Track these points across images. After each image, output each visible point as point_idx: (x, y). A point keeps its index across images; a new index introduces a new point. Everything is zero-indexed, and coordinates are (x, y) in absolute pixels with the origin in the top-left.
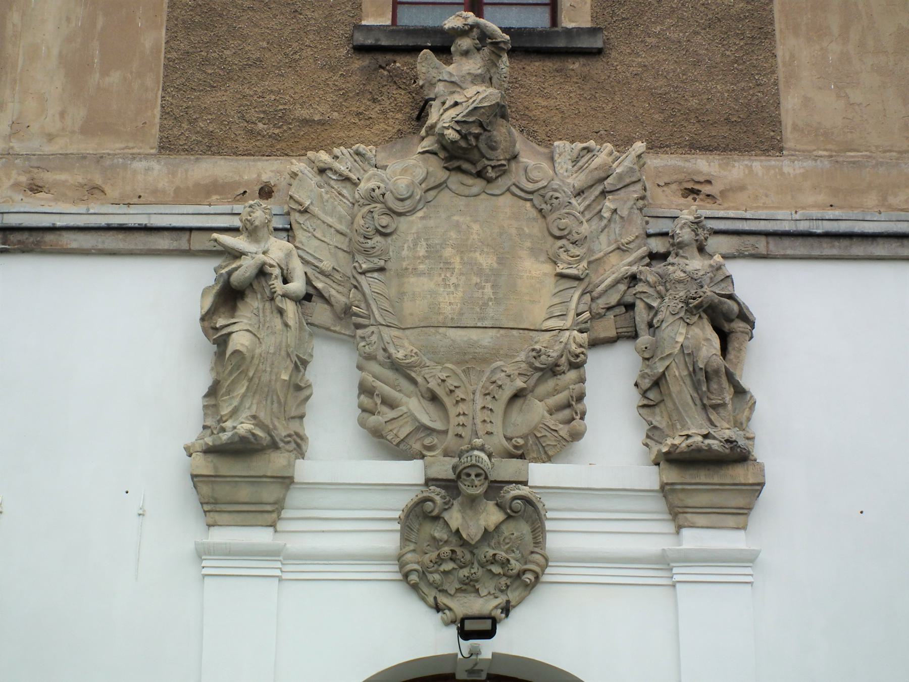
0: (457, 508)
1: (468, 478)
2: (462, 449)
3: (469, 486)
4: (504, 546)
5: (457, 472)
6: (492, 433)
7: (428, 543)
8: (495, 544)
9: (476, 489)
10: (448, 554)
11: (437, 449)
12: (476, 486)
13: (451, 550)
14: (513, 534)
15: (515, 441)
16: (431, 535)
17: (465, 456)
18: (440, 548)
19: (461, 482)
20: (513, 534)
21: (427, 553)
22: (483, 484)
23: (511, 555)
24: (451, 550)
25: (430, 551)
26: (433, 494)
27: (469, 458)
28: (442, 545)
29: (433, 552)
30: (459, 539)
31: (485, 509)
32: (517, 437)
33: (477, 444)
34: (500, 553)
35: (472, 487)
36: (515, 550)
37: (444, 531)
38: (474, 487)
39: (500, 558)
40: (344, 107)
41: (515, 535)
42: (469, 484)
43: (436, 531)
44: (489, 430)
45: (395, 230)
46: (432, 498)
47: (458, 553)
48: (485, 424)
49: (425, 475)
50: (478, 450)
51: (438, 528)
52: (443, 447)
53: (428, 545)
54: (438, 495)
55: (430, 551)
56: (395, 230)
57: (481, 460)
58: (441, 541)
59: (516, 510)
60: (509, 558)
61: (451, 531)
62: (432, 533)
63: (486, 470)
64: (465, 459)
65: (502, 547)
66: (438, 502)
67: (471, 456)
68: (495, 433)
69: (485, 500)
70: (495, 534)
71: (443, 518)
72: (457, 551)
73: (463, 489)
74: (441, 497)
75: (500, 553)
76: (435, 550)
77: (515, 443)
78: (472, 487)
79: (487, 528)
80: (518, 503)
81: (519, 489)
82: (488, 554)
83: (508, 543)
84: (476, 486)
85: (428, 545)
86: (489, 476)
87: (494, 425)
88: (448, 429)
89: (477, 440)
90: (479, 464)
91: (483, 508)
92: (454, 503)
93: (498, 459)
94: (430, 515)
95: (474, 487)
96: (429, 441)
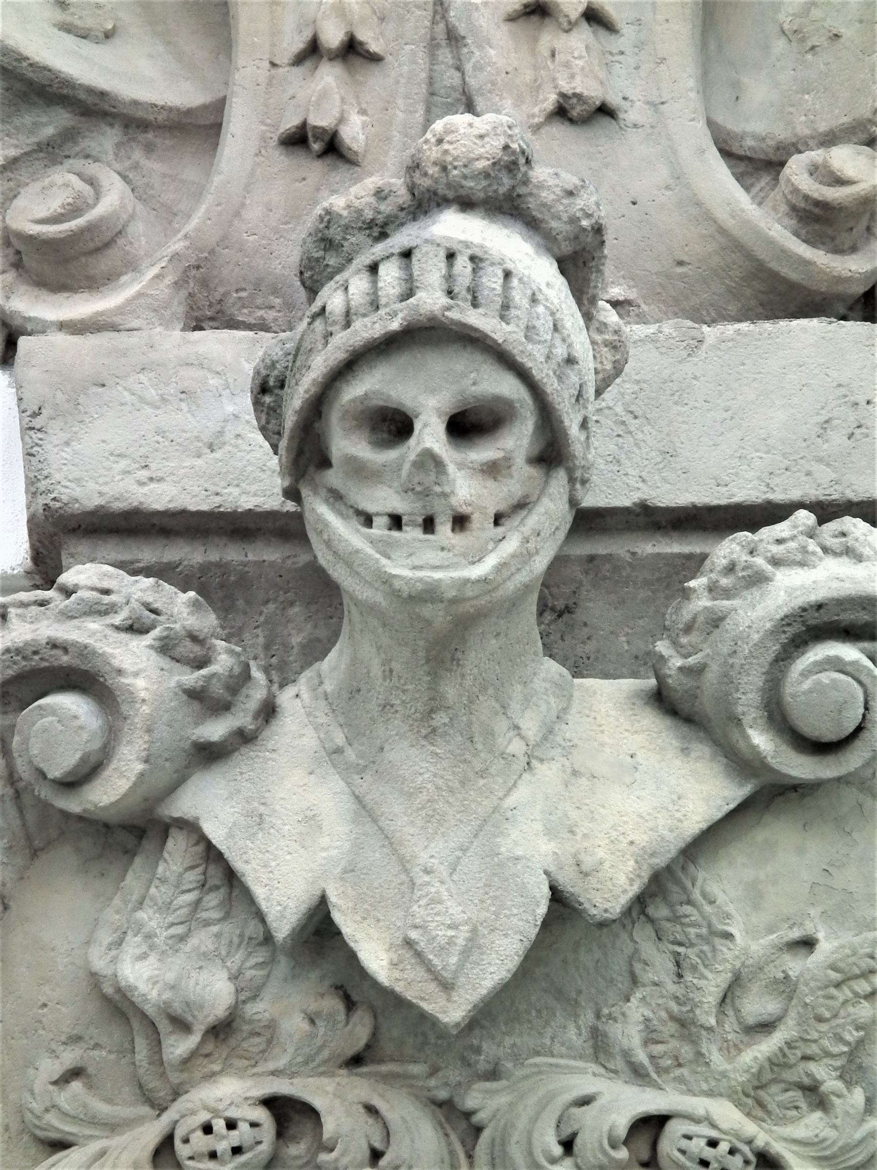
0: (310, 740)
1: (391, 455)
2: (329, 218)
3: (396, 522)
4: (731, 1050)
5: (290, 419)
6: (605, 111)
7: (70, 1057)
8: (650, 1038)
9: (458, 540)
10: (242, 1134)
11: (132, 265)
12: (460, 522)
13: (271, 1103)
14: (808, 944)
15: (814, 170)
16: (94, 979)
17: (364, 259)
18: (177, 1094)
19: (336, 497)
20: (808, 944)
21: (59, 1145)
22: (522, 505)
23: (800, 1131)
24: (271, 1103)
25: (94, 1121)
26: (94, 625)
27: (390, 273)
28: (186, 1062)
29: (113, 1127)
30: (334, 1004)
31: (548, 732)
32: (829, 140)
33: (455, 150)
34: (699, 1105)
35: (429, 525)
36: (831, 1084)
37: (203, 939)
38: (444, 529)
39: (698, 1146)
40: (591, 891)
41: (825, 947)
42: (398, 504)
43: (133, 945)
44: (579, 86)
45: (379, 654)
46: (84, 651)
47: (329, 1126)
48: (548, 38)
49: (31, 483)
50: (466, 204)
51: (149, 917)
52: (177, 245)
53: (76, 1073)
54: (135, 628)
55: (94, 1121)
56: (379, 654)
57: (492, 281)
58: (182, 1025)
59: (828, 733)
60: (779, 1148)
61: (268, 939)
62: (99, 963)
63: (543, 373)
64: (359, 285)
65: (716, 1058)
66: (141, 685)
67: (407, 254)
68: (632, 114)
69: (552, 668)
70: (643, 935)
71: (191, 827)
72: (317, 1103)
73: (349, 559)
74: (165, 648)
75: (699, 1105)
76: (146, 1110)
77: (808, 185)
78: (429, 525)
79: (568, 881)
80: (837, 665)
81: (849, 552)
82: (587, 1114)
83: (766, 1027)
84: (460, 522)
85: (76, 1073)
86: (574, 430)
87: (628, 35)
88: (219, 106)
89: (461, 120)
90: (475, 318)
91: (531, 726)
92: (285, 698)
93: (668, 327)
94: (73, 804)
95: (444, 529)
96: (55, 204)
